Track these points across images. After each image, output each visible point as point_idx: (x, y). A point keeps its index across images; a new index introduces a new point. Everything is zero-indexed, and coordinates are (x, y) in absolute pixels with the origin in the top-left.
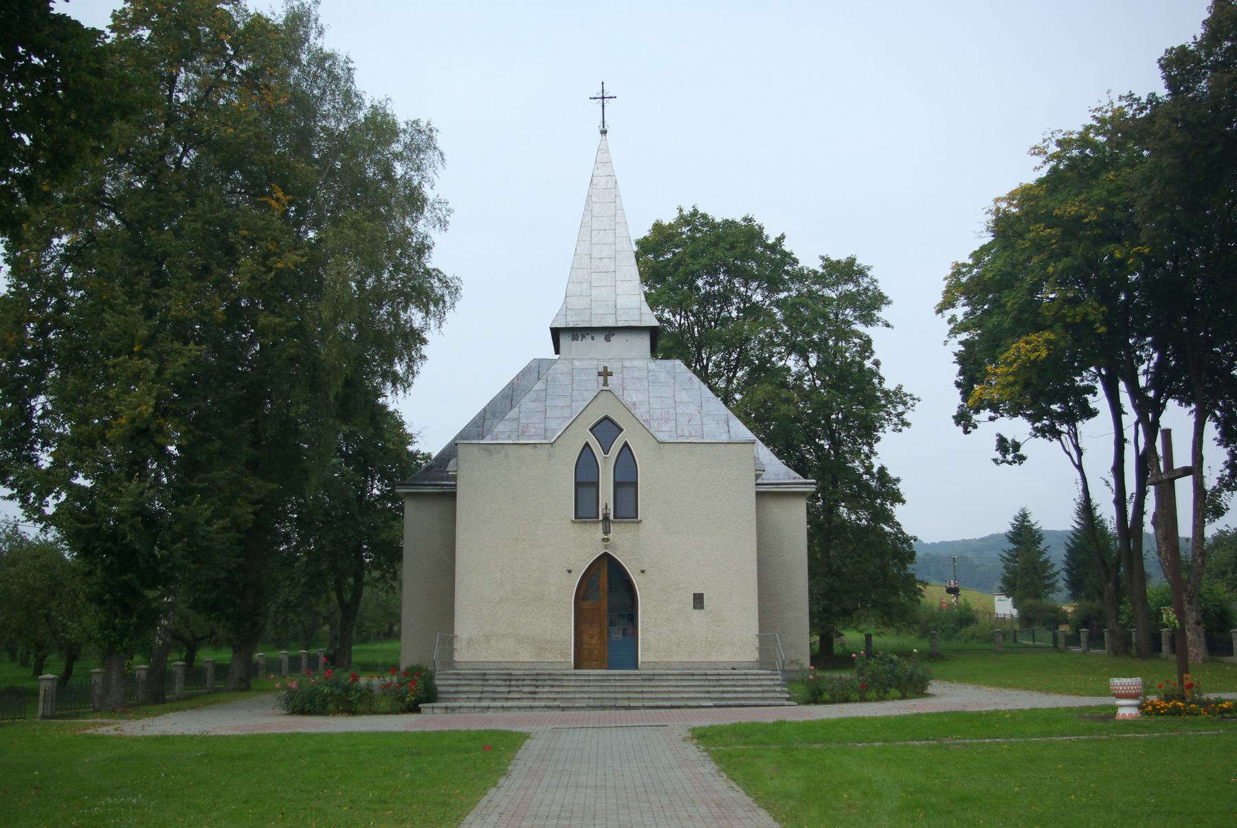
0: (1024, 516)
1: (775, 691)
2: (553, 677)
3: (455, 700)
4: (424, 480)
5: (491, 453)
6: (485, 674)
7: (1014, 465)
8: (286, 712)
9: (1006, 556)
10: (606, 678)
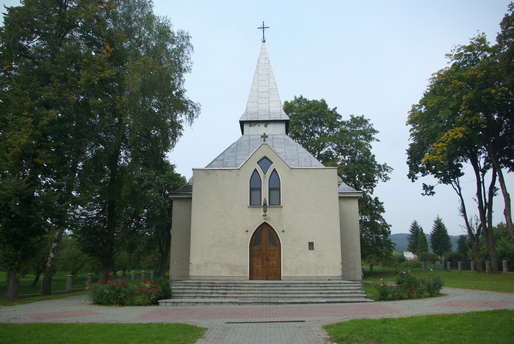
0: (416, 223)
1: (358, 293)
2: (236, 285)
3: (182, 297)
4: (182, 192)
5: (209, 174)
6: (200, 283)
7: (430, 196)
8: (92, 302)
9: (409, 237)
10: (264, 286)
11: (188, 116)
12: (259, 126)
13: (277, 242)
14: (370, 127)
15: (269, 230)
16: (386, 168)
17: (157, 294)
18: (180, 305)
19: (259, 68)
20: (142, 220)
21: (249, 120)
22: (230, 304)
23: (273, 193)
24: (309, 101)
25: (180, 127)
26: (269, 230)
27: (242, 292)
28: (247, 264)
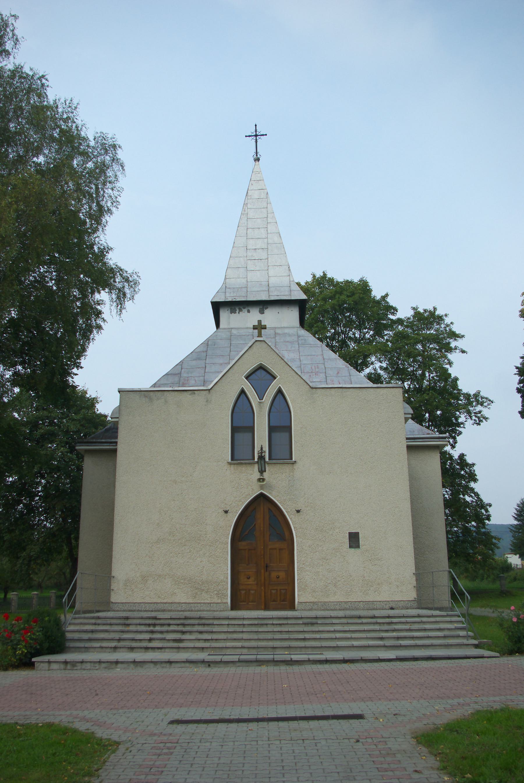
1: (458, 636)
2: (203, 621)
3: (87, 649)
4: (102, 439)
5: (151, 399)
6: (127, 618)
9: (513, 529)
10: (261, 622)
11: (114, 296)
12: (249, 311)
13: (287, 534)
14: (448, 328)
15: (269, 509)
16: (480, 400)
17: (30, 644)
18: (79, 668)
19: (249, 206)
20: (37, 498)
21: (231, 300)
22: (187, 665)
23: (276, 436)
24: (338, 283)
25: (99, 313)
26: (269, 509)
27: (215, 636)
28: (227, 578)
